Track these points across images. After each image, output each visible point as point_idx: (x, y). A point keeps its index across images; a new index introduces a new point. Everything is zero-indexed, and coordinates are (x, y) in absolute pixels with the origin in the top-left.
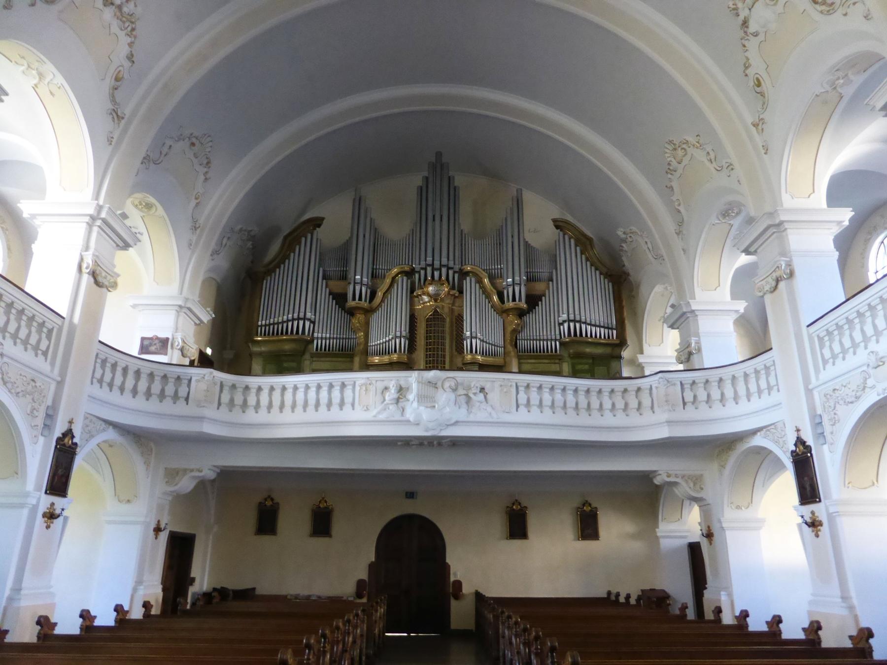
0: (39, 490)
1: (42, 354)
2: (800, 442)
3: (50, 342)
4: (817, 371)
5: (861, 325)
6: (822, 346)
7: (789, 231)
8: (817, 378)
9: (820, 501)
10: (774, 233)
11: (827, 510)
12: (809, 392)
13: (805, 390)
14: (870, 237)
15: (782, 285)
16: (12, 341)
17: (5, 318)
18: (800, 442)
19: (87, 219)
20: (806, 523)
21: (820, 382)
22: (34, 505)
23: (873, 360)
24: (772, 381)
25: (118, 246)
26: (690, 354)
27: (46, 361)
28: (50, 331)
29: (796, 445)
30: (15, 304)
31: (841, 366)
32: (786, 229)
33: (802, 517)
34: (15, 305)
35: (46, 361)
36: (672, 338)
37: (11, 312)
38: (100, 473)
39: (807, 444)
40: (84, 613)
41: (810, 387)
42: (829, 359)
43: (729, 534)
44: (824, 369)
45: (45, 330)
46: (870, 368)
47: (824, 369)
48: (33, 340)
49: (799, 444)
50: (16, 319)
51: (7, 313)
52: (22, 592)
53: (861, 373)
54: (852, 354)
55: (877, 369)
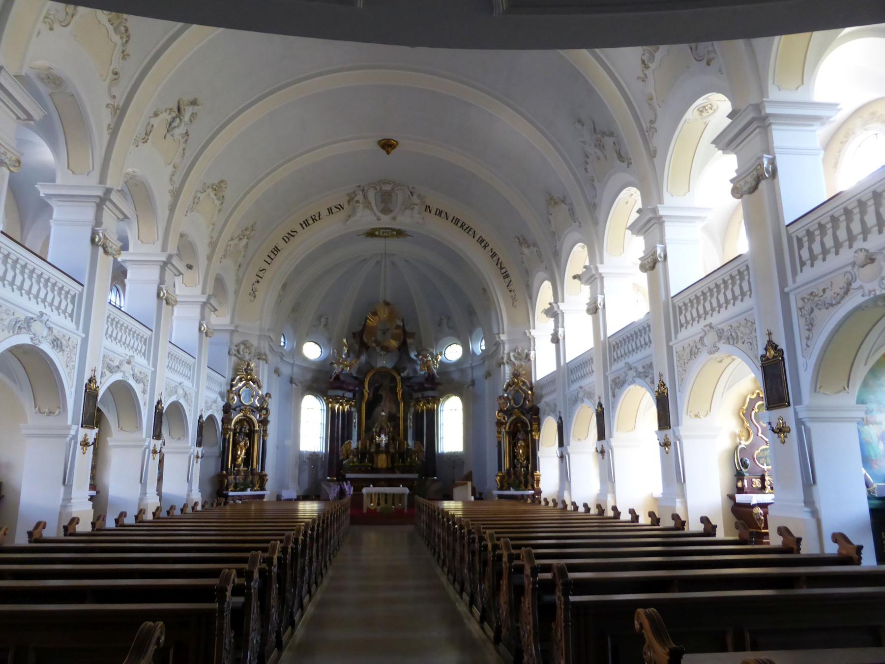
0: (150, 437)
1: (34, 297)
2: (771, 345)
3: (74, 307)
4: (794, 274)
5: (861, 215)
6: (681, 313)
7: (773, 127)
8: (794, 282)
9: (789, 405)
10: (655, 223)
11: (796, 413)
12: (785, 296)
13: (781, 294)
14: (846, 139)
15: (763, 185)
16: (10, 287)
17: (4, 268)
18: (771, 345)
19: (98, 200)
20: (773, 430)
21: (677, 340)
22: (73, 435)
23: (862, 256)
24: (746, 287)
25: (118, 218)
26: (655, 262)
27: (72, 321)
28: (73, 297)
29: (766, 349)
30: (28, 265)
31: (821, 267)
32: (770, 124)
33: (770, 423)
34: (28, 266)
35: (72, 321)
36: (637, 246)
37: (25, 272)
38: (15, 382)
39: (779, 348)
40: (76, 520)
41: (786, 290)
42: (845, 241)
43: (685, 442)
44: (801, 271)
45: (69, 296)
46: (856, 267)
47: (801, 271)
48: (34, 291)
49: (769, 347)
50: (28, 278)
51: (5, 263)
52: (72, 501)
53: (845, 274)
54: (834, 254)
55: (865, 267)
